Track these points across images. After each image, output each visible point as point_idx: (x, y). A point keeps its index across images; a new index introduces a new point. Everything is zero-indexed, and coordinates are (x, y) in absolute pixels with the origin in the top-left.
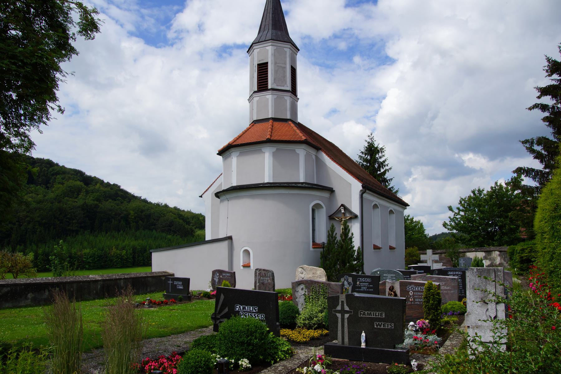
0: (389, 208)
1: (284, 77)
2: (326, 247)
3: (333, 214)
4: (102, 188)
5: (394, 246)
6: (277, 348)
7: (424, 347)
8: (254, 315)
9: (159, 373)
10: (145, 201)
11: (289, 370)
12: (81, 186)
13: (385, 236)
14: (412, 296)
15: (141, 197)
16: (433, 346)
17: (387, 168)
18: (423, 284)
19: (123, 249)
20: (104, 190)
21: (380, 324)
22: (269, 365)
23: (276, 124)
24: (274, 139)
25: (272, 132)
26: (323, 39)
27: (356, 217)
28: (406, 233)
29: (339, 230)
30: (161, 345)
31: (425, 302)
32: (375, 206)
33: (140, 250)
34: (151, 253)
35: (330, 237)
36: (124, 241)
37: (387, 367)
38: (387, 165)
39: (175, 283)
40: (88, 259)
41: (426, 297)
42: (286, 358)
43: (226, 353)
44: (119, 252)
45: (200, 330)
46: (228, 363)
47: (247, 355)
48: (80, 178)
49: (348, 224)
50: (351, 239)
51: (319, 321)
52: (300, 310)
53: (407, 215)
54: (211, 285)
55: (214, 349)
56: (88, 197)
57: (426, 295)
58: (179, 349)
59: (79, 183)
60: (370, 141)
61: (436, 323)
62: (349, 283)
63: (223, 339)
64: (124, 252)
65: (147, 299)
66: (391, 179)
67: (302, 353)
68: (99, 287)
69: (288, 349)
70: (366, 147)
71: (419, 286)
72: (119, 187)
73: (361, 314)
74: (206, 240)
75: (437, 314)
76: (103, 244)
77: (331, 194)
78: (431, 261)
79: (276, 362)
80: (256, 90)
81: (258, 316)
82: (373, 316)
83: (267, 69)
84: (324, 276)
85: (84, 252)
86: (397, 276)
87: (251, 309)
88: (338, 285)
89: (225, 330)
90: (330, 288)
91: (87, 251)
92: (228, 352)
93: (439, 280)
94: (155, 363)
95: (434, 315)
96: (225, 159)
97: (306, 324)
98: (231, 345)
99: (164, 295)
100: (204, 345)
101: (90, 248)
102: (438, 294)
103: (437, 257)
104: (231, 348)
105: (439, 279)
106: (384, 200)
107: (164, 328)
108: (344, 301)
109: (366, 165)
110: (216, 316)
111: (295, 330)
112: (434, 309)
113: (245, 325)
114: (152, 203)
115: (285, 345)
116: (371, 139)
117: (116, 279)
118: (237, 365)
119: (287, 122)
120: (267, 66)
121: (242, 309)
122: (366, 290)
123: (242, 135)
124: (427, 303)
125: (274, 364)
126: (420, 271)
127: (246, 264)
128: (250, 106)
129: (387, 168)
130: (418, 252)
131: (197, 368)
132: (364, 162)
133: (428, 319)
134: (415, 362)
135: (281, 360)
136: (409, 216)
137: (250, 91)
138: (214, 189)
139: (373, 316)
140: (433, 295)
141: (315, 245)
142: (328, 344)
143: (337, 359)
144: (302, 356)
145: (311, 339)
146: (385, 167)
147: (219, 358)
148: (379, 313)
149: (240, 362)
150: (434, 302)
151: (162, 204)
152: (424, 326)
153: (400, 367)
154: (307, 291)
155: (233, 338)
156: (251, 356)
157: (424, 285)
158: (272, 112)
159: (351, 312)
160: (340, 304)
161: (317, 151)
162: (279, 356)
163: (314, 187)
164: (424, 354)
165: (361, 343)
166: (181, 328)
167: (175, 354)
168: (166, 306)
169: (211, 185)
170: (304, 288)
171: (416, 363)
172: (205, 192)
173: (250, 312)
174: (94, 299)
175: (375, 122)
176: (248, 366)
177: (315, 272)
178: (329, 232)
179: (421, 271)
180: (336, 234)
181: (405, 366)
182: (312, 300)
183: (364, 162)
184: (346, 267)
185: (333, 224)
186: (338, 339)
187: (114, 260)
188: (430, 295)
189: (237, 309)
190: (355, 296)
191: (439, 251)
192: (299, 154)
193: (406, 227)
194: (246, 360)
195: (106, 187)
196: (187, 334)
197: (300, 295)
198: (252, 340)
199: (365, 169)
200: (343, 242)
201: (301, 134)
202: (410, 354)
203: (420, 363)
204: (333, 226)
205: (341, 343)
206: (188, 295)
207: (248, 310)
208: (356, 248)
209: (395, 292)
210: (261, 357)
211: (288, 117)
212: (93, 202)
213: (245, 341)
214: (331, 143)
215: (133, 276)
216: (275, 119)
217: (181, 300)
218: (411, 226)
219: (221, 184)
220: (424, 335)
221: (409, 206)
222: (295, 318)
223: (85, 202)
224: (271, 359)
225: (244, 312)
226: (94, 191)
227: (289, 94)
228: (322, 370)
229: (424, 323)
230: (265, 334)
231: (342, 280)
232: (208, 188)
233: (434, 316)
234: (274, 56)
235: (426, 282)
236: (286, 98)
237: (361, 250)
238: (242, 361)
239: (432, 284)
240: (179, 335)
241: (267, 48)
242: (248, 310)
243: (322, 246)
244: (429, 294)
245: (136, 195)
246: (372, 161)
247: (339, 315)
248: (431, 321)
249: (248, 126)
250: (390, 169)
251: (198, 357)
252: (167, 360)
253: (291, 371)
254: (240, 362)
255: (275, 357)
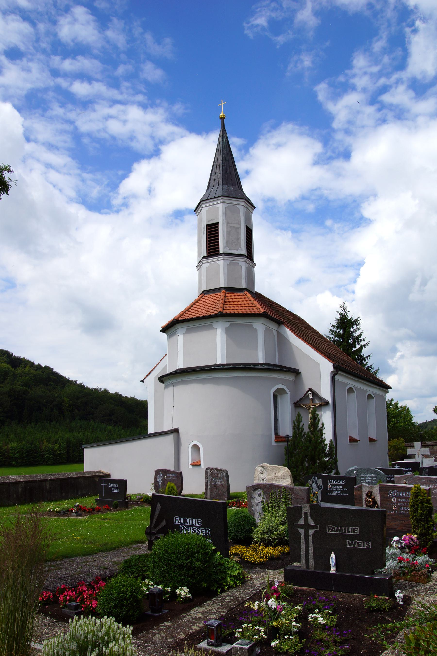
0: (367, 392)
1: (238, 239)
2: (291, 441)
3: (300, 400)
4: (32, 372)
5: (374, 437)
6: (225, 573)
7: (411, 572)
8: (197, 530)
9: (75, 605)
10: (81, 386)
11: (239, 601)
12: (9, 369)
13: (363, 425)
14: (395, 504)
15: (76, 381)
16: (424, 571)
17: (363, 343)
18: (409, 489)
19: (56, 443)
20: (35, 373)
21: (354, 542)
22: (214, 594)
23: (230, 295)
24: (240, 312)
25: (224, 304)
26: (289, 201)
27: (327, 403)
28: (389, 422)
29: (307, 420)
30: (84, 566)
31: (411, 511)
32: (350, 390)
33: (75, 443)
34: (83, 449)
35: (296, 429)
36: (56, 433)
37: (364, 599)
38: (364, 340)
39: (110, 485)
40: (15, 454)
41: (413, 506)
42: (236, 585)
43: (160, 579)
44: (51, 446)
45: (134, 546)
46: (162, 593)
47: (186, 582)
48: (7, 360)
49: (317, 412)
50: (321, 430)
51: (280, 536)
52: (257, 520)
53: (390, 400)
54: (153, 488)
55: (147, 573)
56: (16, 381)
57: (413, 502)
58: (105, 572)
59: (5, 365)
60: (343, 312)
61: (426, 538)
62: (318, 487)
63: (157, 561)
64: (57, 446)
65: (75, 506)
66: (369, 356)
67: (257, 578)
68: (20, 490)
69: (238, 573)
70: (338, 319)
71: (404, 491)
72: (52, 369)
73: (329, 530)
74: (149, 433)
75: (428, 526)
76: (33, 436)
77: (296, 376)
78: (420, 456)
79: (223, 591)
80: (205, 255)
81: (202, 532)
82: (345, 532)
83: (218, 230)
84: (289, 477)
85: (10, 446)
86: (378, 476)
87: (194, 522)
88: (303, 489)
89: (159, 549)
90: (294, 493)
91: (14, 445)
92: (163, 578)
93: (429, 481)
94: (72, 591)
95: (424, 529)
96: (170, 336)
97: (264, 539)
98: (167, 570)
99: (96, 500)
100: (136, 567)
101: (18, 442)
102: (428, 501)
103: (427, 451)
104: (167, 573)
105: (430, 480)
106: (360, 382)
107: (91, 543)
108: (308, 513)
109: (338, 340)
110: (151, 531)
111: (251, 547)
112: (423, 521)
113: (185, 543)
114: (89, 388)
115: (235, 569)
116: (344, 309)
117: (41, 481)
118: (174, 595)
119: (242, 292)
120: (218, 227)
121: (182, 521)
122: (339, 494)
123: (189, 309)
124: (414, 513)
125: (221, 593)
126: (407, 469)
127: (196, 462)
128: (199, 274)
129: (363, 343)
130: (404, 444)
131: (122, 601)
132: (335, 337)
133: (416, 534)
134: (400, 593)
135: (230, 587)
136: (392, 400)
137: (199, 256)
138: (158, 373)
139: (345, 532)
140: (422, 503)
141: (278, 438)
142: (289, 567)
143: (300, 588)
144: (256, 582)
145: (269, 559)
146: (361, 341)
147: (152, 585)
148: (351, 529)
149: (178, 591)
150: (423, 512)
151: (101, 389)
152: (412, 543)
153: (380, 599)
154: (265, 497)
155: (169, 560)
156: (192, 583)
157: (411, 490)
158: (224, 280)
159: (317, 527)
160: (303, 516)
161: (278, 325)
162: (227, 583)
163: (275, 368)
164: (412, 581)
165: (330, 567)
166: (112, 544)
167: (99, 580)
168: (98, 514)
169: (155, 368)
170: (262, 494)
171: (401, 595)
172: (147, 376)
173: (192, 526)
174: (14, 505)
175: (353, 292)
176: (188, 596)
177: (277, 472)
178: (294, 422)
179: (408, 469)
180: (303, 424)
181: (387, 598)
182: (272, 509)
183: (335, 337)
184: (315, 465)
185: (298, 412)
186: (302, 562)
187: (45, 455)
188: (418, 503)
189: (177, 522)
190: (322, 506)
191: (430, 443)
192: (257, 329)
193: (388, 415)
194: (185, 588)
195: (37, 370)
196: (119, 552)
197: (257, 502)
198: (193, 563)
199: (338, 346)
200: (312, 434)
201: (259, 306)
202: (394, 580)
203: (407, 594)
204: (299, 415)
205: (305, 567)
206: (125, 500)
207: (190, 523)
208: (327, 442)
209: (374, 499)
210: (205, 585)
211: (244, 286)
212: (21, 387)
213: (184, 564)
214: (299, 317)
215: (61, 477)
216: (228, 289)
217: (116, 507)
218: (396, 413)
219: (165, 368)
220: (412, 555)
221: (391, 388)
222: (250, 531)
223: (13, 387)
224: (218, 587)
225: (186, 526)
226: (23, 374)
227: (244, 259)
228: (277, 607)
229: (412, 539)
230: (210, 555)
231: (310, 482)
232: (151, 372)
233: (424, 529)
234: (226, 215)
235: (412, 486)
236: (240, 263)
237: (334, 443)
238: (181, 590)
239: (420, 489)
240: (108, 552)
241: (217, 206)
242: (190, 523)
243: (286, 439)
244: (417, 502)
245: (71, 379)
246: (345, 336)
247: (302, 531)
248: (421, 536)
249: (196, 297)
250: (367, 344)
251: (123, 586)
252: (88, 588)
253: (241, 603)
254: (178, 591)
255: (222, 584)
